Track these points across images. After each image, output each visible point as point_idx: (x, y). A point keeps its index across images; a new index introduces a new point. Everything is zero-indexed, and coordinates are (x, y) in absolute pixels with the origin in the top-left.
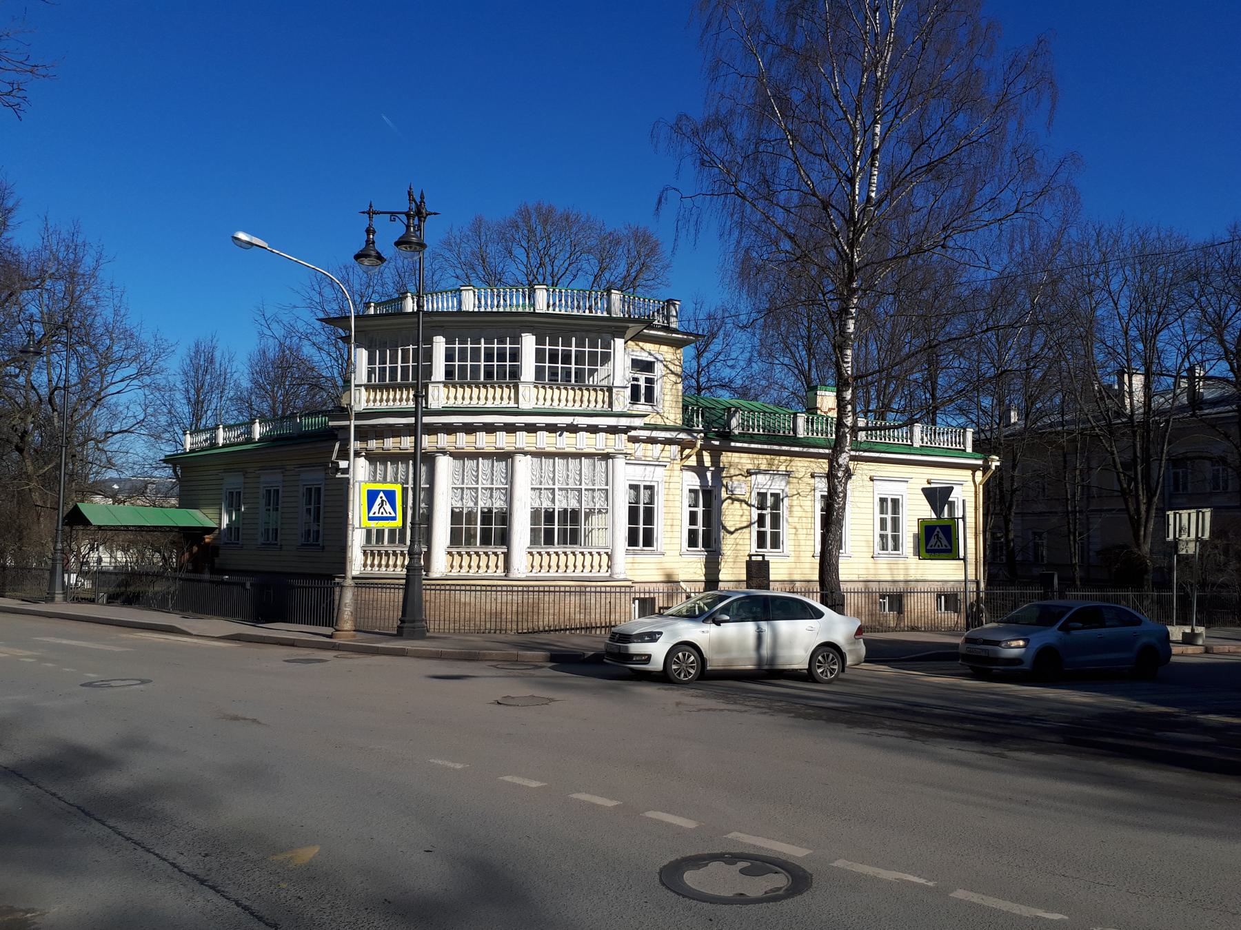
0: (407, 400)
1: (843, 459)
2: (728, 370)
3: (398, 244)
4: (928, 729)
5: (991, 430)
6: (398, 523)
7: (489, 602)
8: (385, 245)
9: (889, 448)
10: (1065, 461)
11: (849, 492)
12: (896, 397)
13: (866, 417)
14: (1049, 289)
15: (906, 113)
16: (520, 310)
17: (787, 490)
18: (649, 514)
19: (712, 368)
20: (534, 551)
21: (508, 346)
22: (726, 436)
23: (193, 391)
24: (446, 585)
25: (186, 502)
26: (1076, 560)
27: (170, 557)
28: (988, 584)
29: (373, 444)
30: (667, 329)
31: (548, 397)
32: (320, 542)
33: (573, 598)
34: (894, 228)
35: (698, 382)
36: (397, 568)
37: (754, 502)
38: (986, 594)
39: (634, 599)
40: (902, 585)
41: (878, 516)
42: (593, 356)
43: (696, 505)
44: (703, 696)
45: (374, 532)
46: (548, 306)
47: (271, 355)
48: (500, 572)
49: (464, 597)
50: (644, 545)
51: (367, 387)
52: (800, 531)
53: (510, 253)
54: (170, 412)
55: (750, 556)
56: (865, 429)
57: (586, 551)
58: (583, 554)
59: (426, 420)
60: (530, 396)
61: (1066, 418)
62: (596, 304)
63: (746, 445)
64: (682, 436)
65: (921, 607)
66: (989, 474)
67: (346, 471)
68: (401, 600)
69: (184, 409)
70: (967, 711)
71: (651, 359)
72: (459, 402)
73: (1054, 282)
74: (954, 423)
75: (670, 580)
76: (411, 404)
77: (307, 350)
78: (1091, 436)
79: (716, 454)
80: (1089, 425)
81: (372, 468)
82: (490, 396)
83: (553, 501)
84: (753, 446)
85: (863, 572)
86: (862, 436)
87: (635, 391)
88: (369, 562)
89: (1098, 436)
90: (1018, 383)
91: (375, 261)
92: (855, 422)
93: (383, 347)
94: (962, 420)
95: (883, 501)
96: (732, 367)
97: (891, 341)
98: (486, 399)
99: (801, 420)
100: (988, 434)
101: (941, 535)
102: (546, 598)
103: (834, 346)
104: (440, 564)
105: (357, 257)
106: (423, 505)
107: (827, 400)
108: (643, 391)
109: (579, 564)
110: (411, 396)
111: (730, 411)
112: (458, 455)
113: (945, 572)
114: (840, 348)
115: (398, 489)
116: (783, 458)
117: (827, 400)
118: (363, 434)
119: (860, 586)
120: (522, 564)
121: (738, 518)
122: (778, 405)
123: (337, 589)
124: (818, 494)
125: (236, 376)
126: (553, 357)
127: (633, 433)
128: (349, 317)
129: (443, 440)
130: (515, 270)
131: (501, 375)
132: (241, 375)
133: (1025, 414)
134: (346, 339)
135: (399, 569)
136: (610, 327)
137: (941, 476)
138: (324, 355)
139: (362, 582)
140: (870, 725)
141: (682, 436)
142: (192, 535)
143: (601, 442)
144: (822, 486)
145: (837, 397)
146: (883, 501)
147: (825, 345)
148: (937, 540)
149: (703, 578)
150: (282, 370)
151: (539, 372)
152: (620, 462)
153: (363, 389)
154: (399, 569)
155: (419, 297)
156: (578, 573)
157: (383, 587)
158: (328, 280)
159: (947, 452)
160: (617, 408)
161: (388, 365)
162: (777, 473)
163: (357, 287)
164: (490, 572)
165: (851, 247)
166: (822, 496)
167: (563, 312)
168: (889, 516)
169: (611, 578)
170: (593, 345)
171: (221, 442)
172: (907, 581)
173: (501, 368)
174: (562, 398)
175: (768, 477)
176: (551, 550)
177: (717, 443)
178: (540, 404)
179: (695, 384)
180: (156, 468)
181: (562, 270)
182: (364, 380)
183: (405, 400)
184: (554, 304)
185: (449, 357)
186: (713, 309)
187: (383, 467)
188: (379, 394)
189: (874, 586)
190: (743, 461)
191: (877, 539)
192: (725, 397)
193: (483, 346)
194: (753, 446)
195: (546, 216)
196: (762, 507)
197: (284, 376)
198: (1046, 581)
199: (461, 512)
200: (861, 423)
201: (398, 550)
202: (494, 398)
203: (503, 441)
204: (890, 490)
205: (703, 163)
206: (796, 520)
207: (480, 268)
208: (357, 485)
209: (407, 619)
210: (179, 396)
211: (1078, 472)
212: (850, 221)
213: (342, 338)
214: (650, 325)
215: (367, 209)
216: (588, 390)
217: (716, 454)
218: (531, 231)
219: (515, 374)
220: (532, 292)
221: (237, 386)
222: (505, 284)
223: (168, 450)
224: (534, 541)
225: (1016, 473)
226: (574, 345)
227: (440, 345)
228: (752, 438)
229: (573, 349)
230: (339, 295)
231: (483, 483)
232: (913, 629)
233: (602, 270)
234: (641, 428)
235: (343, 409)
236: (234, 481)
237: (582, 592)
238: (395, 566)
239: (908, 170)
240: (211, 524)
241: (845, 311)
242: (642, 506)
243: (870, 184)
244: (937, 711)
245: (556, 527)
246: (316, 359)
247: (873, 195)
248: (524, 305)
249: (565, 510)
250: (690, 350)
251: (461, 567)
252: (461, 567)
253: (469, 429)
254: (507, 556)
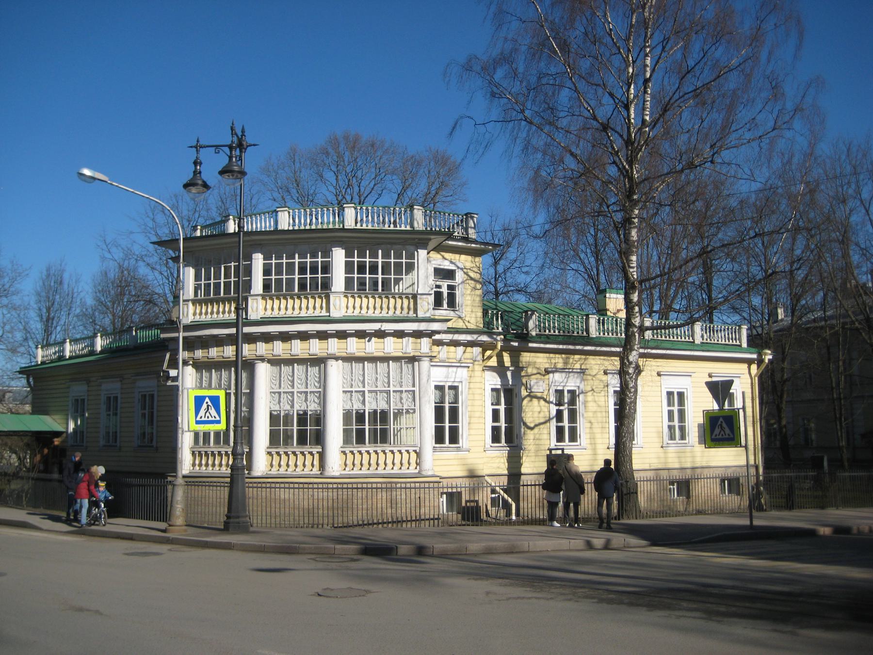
0: (230, 312)
1: (633, 356)
2: (523, 276)
3: (222, 173)
4: (722, 609)
5: (762, 326)
6: (222, 426)
7: (303, 499)
8: (210, 174)
9: (674, 345)
10: (829, 353)
11: (639, 388)
12: (678, 298)
13: (650, 316)
14: (808, 197)
15: (672, 48)
16: (331, 226)
17: (582, 387)
18: (454, 412)
19: (508, 274)
20: (347, 451)
21: (320, 260)
22: (524, 337)
23: (45, 310)
24: (268, 482)
25: (39, 409)
26: (843, 443)
27: (25, 458)
28: (766, 468)
29: (199, 354)
30: (466, 239)
31: (357, 305)
32: (154, 443)
33: (384, 494)
34: (666, 147)
35: (496, 288)
36: (222, 468)
37: (552, 398)
38: (764, 478)
39: (442, 493)
40: (689, 472)
41: (666, 409)
42: (398, 266)
43: (498, 403)
44: (511, 585)
45: (201, 434)
46: (356, 223)
47: (111, 275)
48: (316, 471)
49: (284, 494)
50: (450, 443)
51: (194, 302)
52: (595, 425)
53: (321, 176)
54: (25, 329)
55: (550, 450)
56: (652, 328)
57: (395, 450)
58: (392, 452)
59: (247, 330)
60: (340, 305)
61: (828, 313)
62: (400, 218)
63: (542, 346)
64: (485, 338)
65: (706, 491)
66: (763, 366)
67: (175, 379)
68: (227, 497)
69: (37, 326)
70: (756, 590)
71: (452, 267)
73: (812, 192)
74: (729, 321)
75: (472, 475)
76: (233, 316)
77: (143, 270)
78: (851, 329)
79: (515, 355)
80: (848, 320)
81: (199, 375)
82: (304, 306)
83: (364, 403)
84: (548, 346)
85: (655, 461)
86: (648, 334)
87: (438, 297)
88: (197, 462)
89: (857, 329)
90: (783, 283)
91: (201, 189)
92: (642, 321)
93: (208, 265)
94: (737, 318)
95: (670, 394)
96: (527, 273)
97: (670, 247)
98: (300, 309)
99: (593, 321)
100: (760, 330)
101: (724, 425)
102: (360, 494)
103: (620, 253)
104: (261, 464)
105: (186, 186)
106: (244, 409)
107: (615, 302)
108: (445, 295)
109: (389, 462)
110: (233, 309)
111: (527, 314)
112: (276, 362)
113: (727, 458)
114: (625, 254)
115: (221, 394)
116: (577, 357)
117: (615, 302)
118: (191, 344)
119: (650, 474)
120: (335, 464)
121: (536, 415)
122: (571, 308)
123: (170, 487)
124: (611, 390)
125: (82, 294)
126: (362, 268)
127: (437, 337)
128: (178, 240)
129: (262, 348)
130: (326, 192)
131: (314, 286)
132: (86, 294)
133: (792, 310)
134: (176, 259)
135: (224, 468)
136: (414, 239)
137: (722, 371)
138: (157, 273)
139: (192, 480)
140: (668, 607)
141: (485, 338)
142: (42, 439)
143: (408, 346)
144: (615, 382)
145: (625, 299)
146: (670, 394)
147: (610, 252)
148: (720, 429)
149: (506, 472)
150: (122, 288)
151: (349, 282)
152: (425, 364)
153: (190, 304)
154: (224, 468)
155: (240, 219)
156: (389, 470)
157: (210, 485)
158: (160, 208)
159: (725, 347)
160: (421, 314)
161: (212, 281)
162: (571, 371)
163: (185, 213)
164: (307, 471)
165: (631, 164)
166: (615, 392)
167: (370, 227)
168: (675, 409)
169: (419, 475)
170: (398, 256)
171: (68, 354)
172: (693, 468)
173: (314, 280)
174: (367, 306)
175: (564, 375)
176: (363, 450)
177: (516, 344)
178: (350, 312)
179: (493, 289)
180: (13, 379)
181: (368, 190)
182: (191, 295)
183: (228, 313)
184: (362, 220)
185: (267, 271)
186: (507, 221)
187: (208, 374)
188: (204, 308)
189: (664, 475)
190: (538, 360)
191: (666, 430)
192: (521, 300)
193: (297, 260)
194: (548, 346)
195: (353, 143)
196: (559, 403)
197: (122, 294)
198: (817, 463)
199: (279, 415)
200: (648, 323)
201: (223, 451)
202: (307, 308)
203: (316, 347)
204: (675, 384)
205: (493, 95)
206: (591, 414)
207: (295, 191)
208: (185, 391)
209: (233, 514)
210: (33, 314)
211: (841, 363)
212: (628, 142)
213: (172, 258)
214: (450, 236)
215: (194, 144)
216: (394, 297)
217: (515, 355)
218: (340, 156)
219: (326, 285)
220: (342, 209)
221: (83, 304)
222: (317, 205)
223: (24, 362)
224: (347, 441)
225: (786, 365)
226: (381, 254)
227: (258, 261)
228: (548, 339)
229: (380, 260)
230: (170, 220)
231: (299, 387)
232: (699, 512)
233: (404, 189)
234: (445, 332)
235: (172, 322)
236: (79, 389)
237: (390, 488)
238: (221, 465)
239: (676, 96)
240: (59, 428)
241: (627, 221)
242: (447, 406)
243: (644, 109)
244: (729, 591)
245: (367, 427)
246: (150, 278)
247: (647, 118)
248: (334, 222)
249: (375, 411)
250: (488, 258)
251: (280, 466)
252: (280, 466)
253: (285, 337)
254: (322, 456)
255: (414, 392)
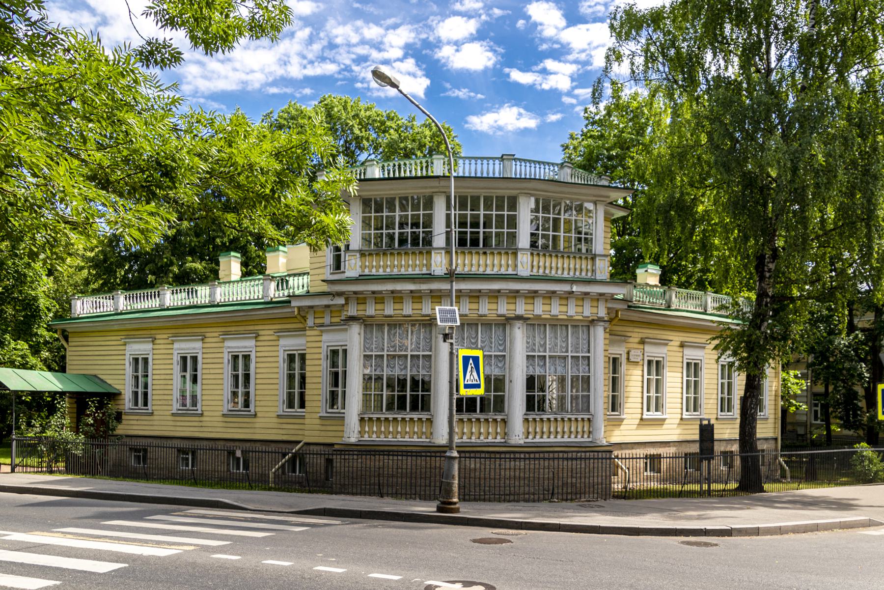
20: (530, 418)
60: (525, 264)
72: (474, 270)
102: (419, 462)
219: (428, 242)
255: (589, 357)
